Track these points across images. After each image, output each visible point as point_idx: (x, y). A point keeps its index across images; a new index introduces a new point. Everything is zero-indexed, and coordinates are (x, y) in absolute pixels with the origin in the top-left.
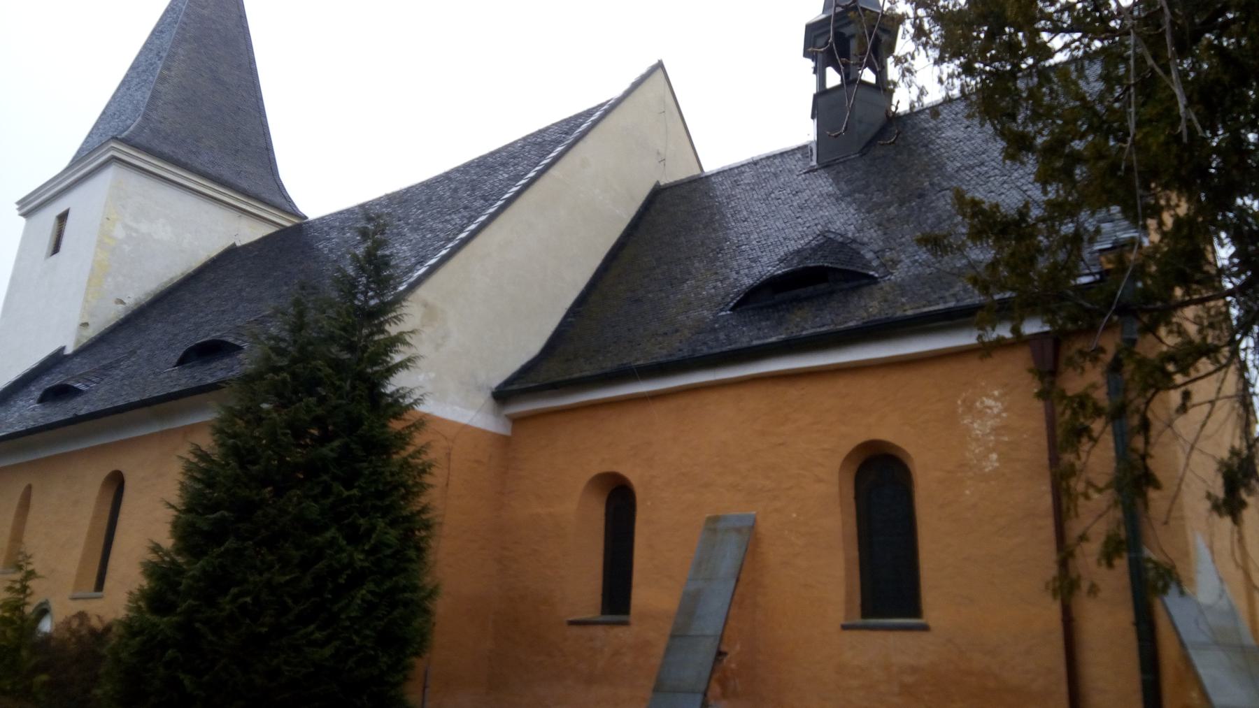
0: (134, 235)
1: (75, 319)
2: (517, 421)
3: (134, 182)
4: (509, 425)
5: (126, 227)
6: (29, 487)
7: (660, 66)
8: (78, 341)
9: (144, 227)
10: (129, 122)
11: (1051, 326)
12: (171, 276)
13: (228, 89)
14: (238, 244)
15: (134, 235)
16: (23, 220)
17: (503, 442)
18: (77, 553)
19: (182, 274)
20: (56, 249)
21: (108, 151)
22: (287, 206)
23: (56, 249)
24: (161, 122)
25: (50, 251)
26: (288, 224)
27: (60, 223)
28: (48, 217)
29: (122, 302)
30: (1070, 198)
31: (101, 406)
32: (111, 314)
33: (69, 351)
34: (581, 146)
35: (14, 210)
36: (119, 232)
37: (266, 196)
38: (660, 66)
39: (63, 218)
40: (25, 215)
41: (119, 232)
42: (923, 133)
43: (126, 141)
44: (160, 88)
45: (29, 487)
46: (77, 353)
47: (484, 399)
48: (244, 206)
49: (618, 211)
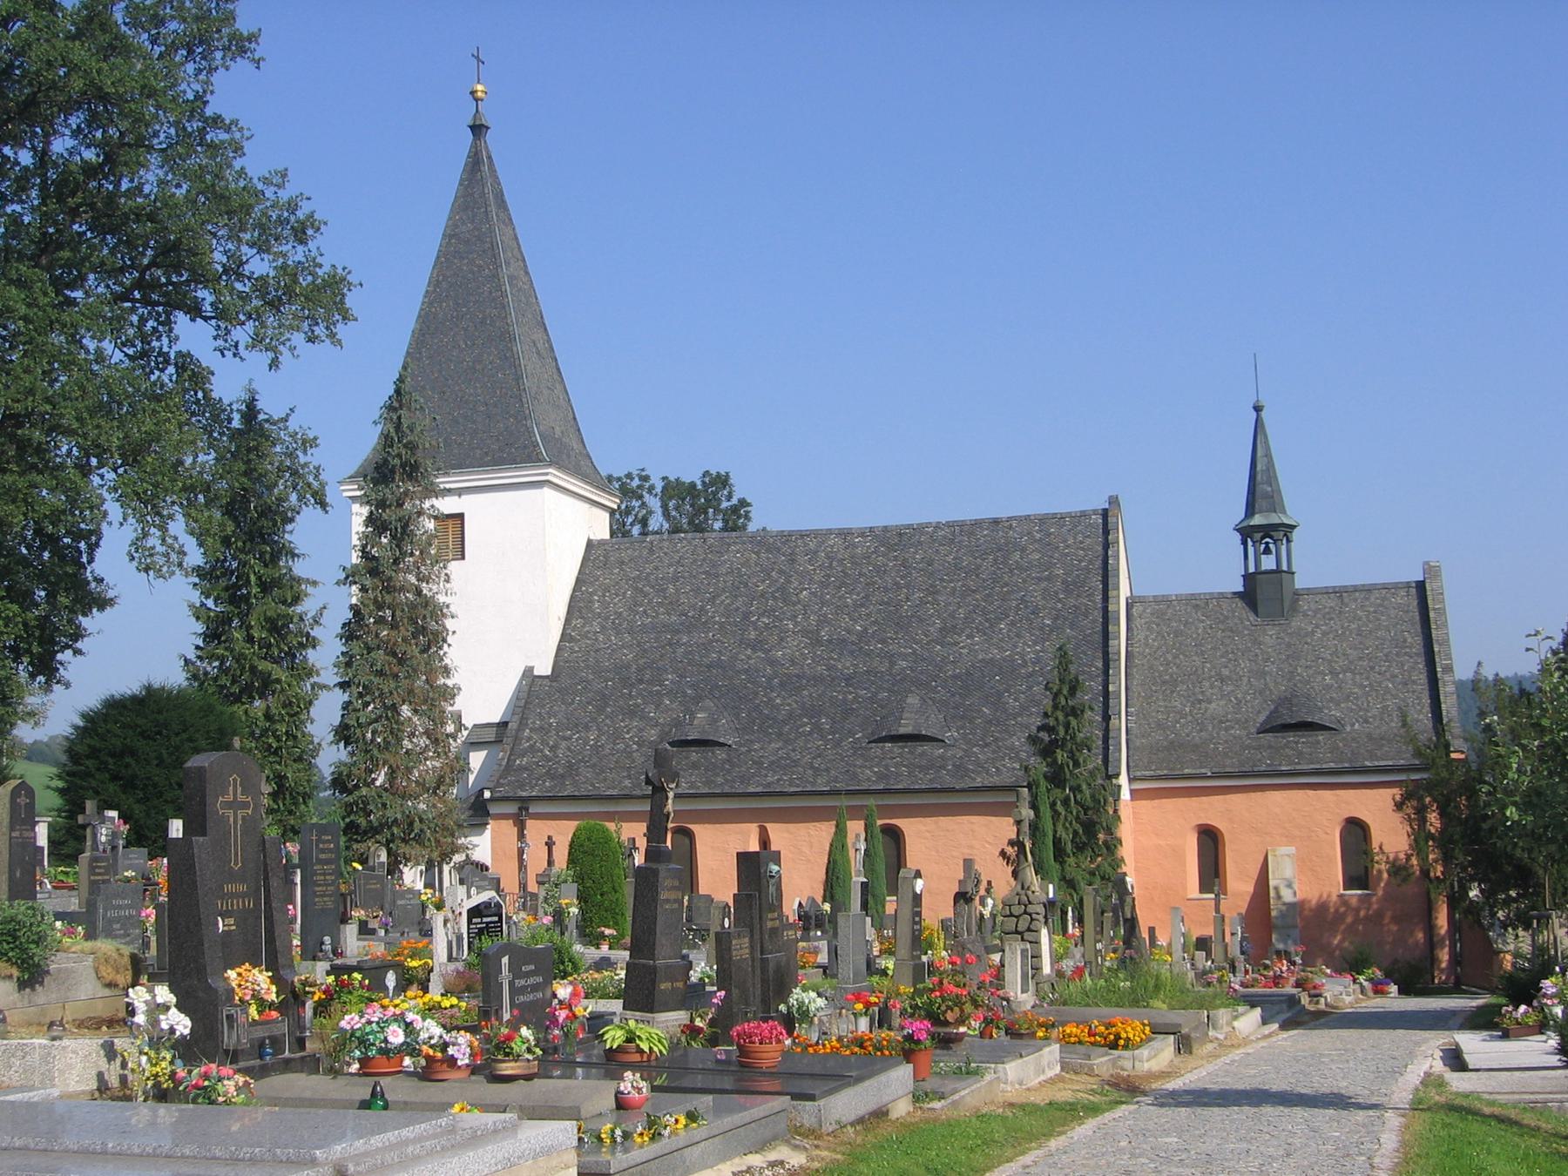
33: (544, 668)
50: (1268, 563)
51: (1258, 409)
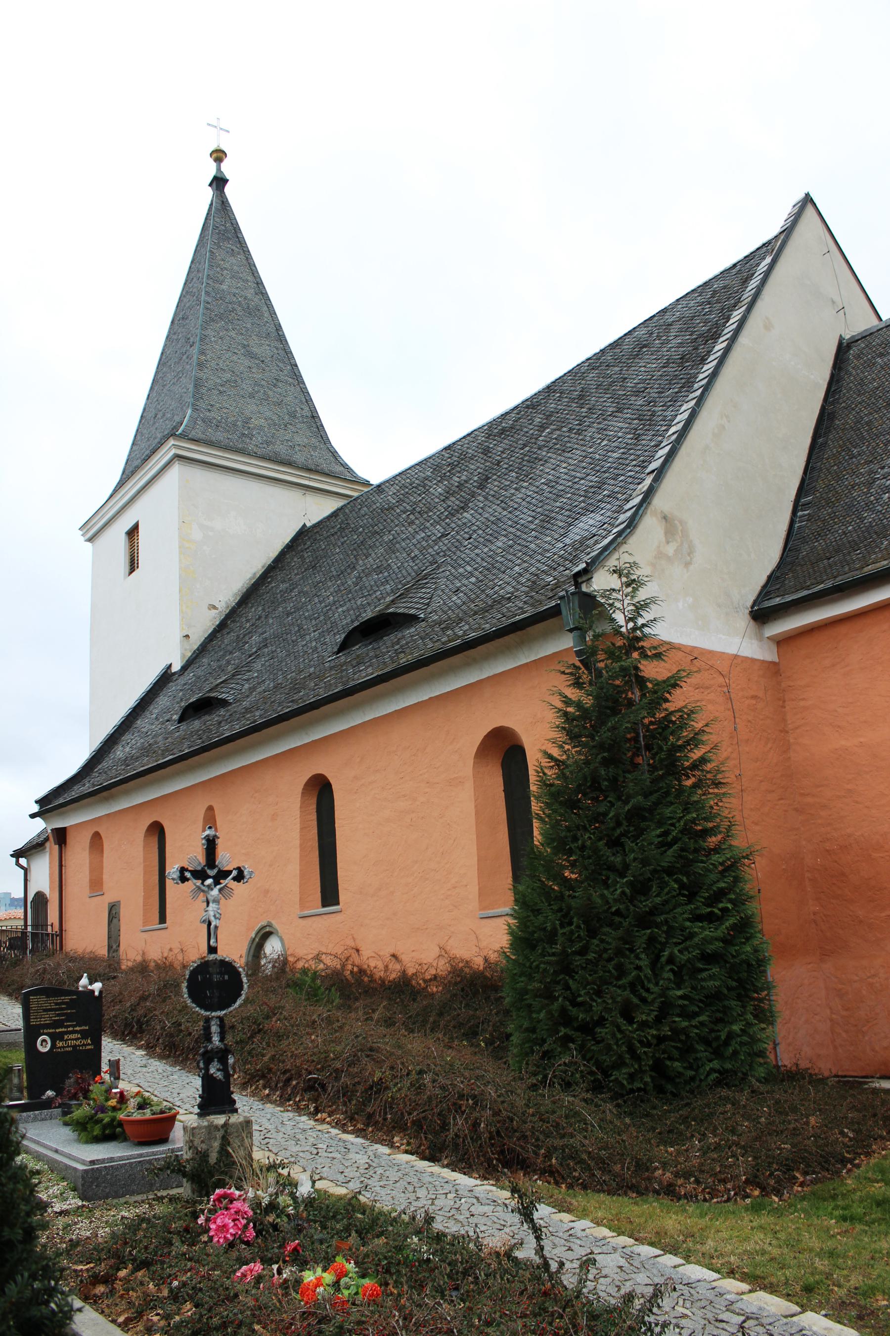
0: (211, 534)
2: (782, 642)
4: (774, 648)
6: (210, 809)
7: (808, 200)
8: (183, 655)
10: (177, 419)
12: (254, 570)
13: (263, 361)
14: (308, 525)
15: (211, 534)
16: (89, 544)
17: (773, 669)
18: (294, 868)
19: (263, 567)
20: (133, 565)
22: (347, 475)
23: (133, 565)
24: (209, 410)
25: (127, 573)
26: (356, 494)
27: (129, 539)
28: (118, 533)
29: (214, 607)
32: (205, 623)
33: (176, 668)
34: (760, 305)
35: (79, 538)
36: (197, 535)
37: (325, 467)
38: (808, 200)
39: (133, 533)
40: (90, 540)
41: (197, 535)
44: (201, 375)
45: (210, 809)
46: (184, 668)
47: (743, 621)
49: (812, 377)
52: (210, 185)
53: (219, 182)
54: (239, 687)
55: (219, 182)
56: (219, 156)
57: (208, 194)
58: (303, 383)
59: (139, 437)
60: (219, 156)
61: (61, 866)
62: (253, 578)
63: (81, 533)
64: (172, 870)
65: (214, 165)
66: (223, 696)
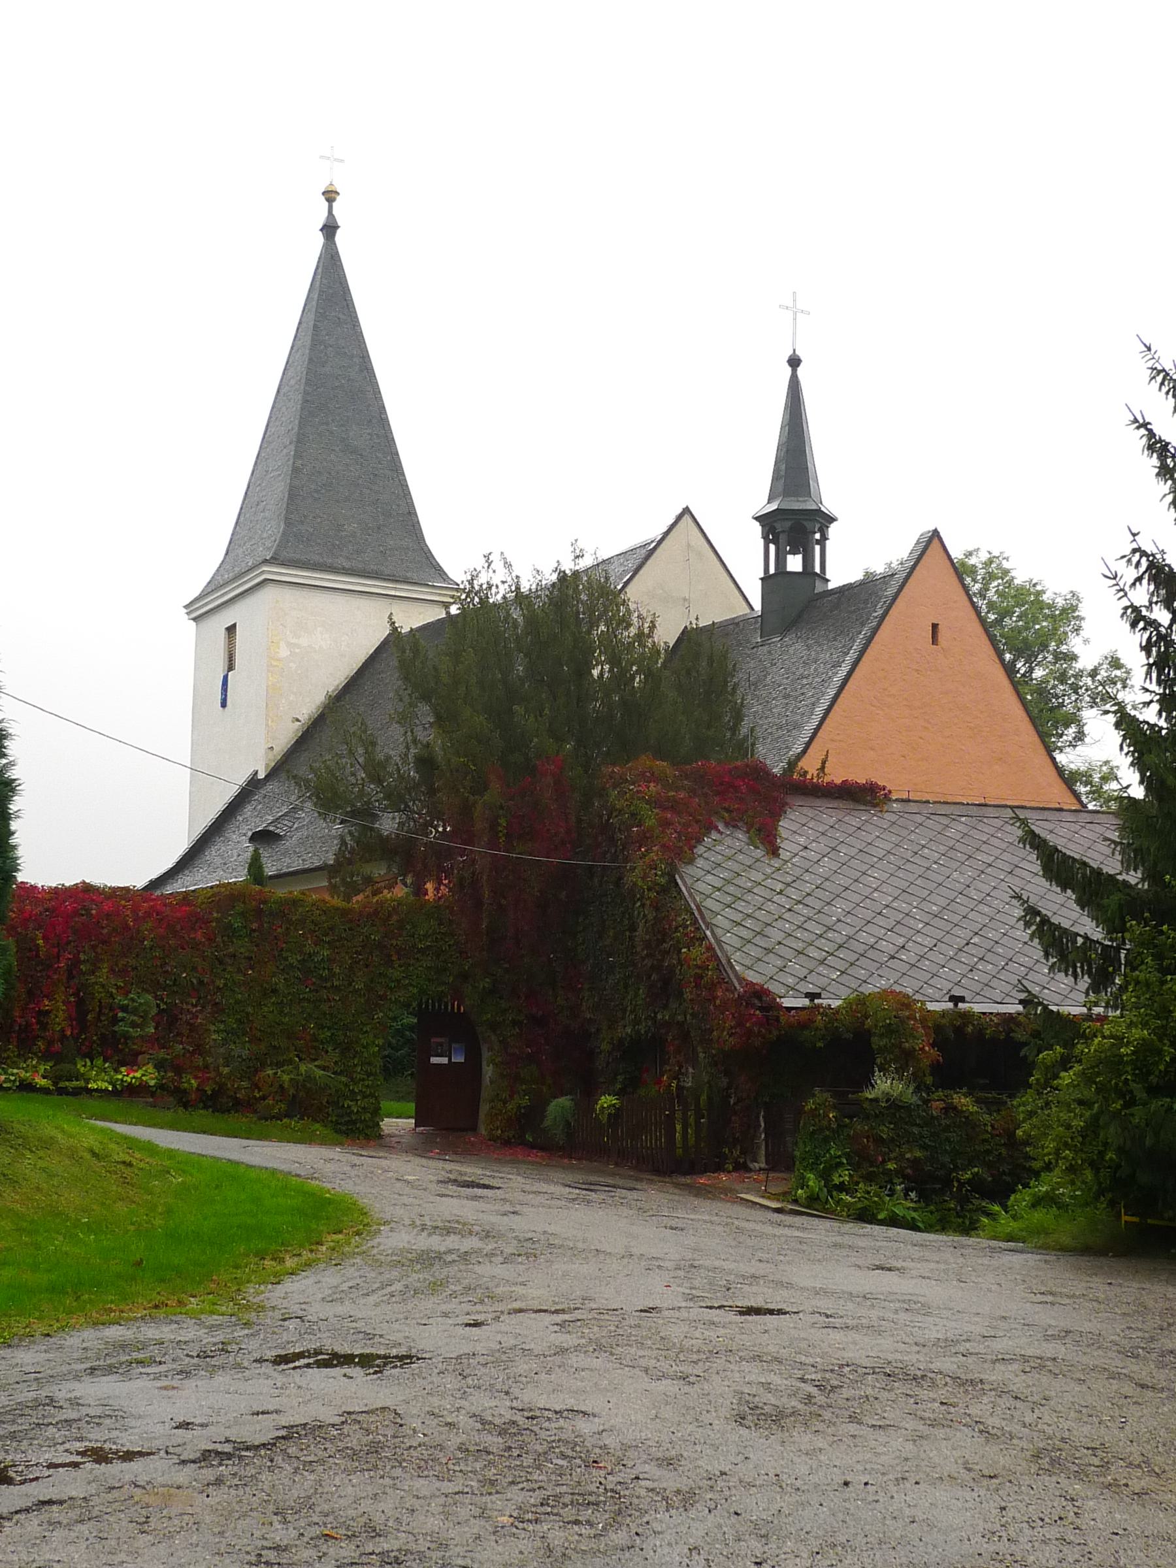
0: (297, 651)
1: (261, 751)
3: (288, 597)
5: (289, 644)
9: (304, 641)
11: (1024, 1008)
12: (336, 683)
15: (297, 651)
16: (193, 624)
21: (263, 572)
29: (298, 720)
30: (1140, 886)
31: (297, 865)
33: (261, 775)
36: (284, 652)
39: (231, 630)
40: (194, 619)
42: (909, 1171)
43: (274, 560)
46: (268, 777)
48: (393, 593)
50: (794, 563)
51: (794, 362)
52: (321, 230)
53: (330, 229)
54: (290, 824)
55: (330, 229)
56: (330, 196)
57: (319, 240)
58: (403, 474)
59: (242, 519)
60: (330, 196)
61: (794, 334)
62: (336, 690)
63: (186, 611)
64: (1030, 894)
65: (327, 204)
66: (278, 831)
